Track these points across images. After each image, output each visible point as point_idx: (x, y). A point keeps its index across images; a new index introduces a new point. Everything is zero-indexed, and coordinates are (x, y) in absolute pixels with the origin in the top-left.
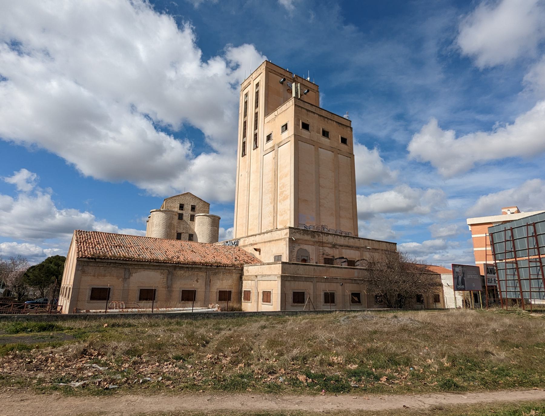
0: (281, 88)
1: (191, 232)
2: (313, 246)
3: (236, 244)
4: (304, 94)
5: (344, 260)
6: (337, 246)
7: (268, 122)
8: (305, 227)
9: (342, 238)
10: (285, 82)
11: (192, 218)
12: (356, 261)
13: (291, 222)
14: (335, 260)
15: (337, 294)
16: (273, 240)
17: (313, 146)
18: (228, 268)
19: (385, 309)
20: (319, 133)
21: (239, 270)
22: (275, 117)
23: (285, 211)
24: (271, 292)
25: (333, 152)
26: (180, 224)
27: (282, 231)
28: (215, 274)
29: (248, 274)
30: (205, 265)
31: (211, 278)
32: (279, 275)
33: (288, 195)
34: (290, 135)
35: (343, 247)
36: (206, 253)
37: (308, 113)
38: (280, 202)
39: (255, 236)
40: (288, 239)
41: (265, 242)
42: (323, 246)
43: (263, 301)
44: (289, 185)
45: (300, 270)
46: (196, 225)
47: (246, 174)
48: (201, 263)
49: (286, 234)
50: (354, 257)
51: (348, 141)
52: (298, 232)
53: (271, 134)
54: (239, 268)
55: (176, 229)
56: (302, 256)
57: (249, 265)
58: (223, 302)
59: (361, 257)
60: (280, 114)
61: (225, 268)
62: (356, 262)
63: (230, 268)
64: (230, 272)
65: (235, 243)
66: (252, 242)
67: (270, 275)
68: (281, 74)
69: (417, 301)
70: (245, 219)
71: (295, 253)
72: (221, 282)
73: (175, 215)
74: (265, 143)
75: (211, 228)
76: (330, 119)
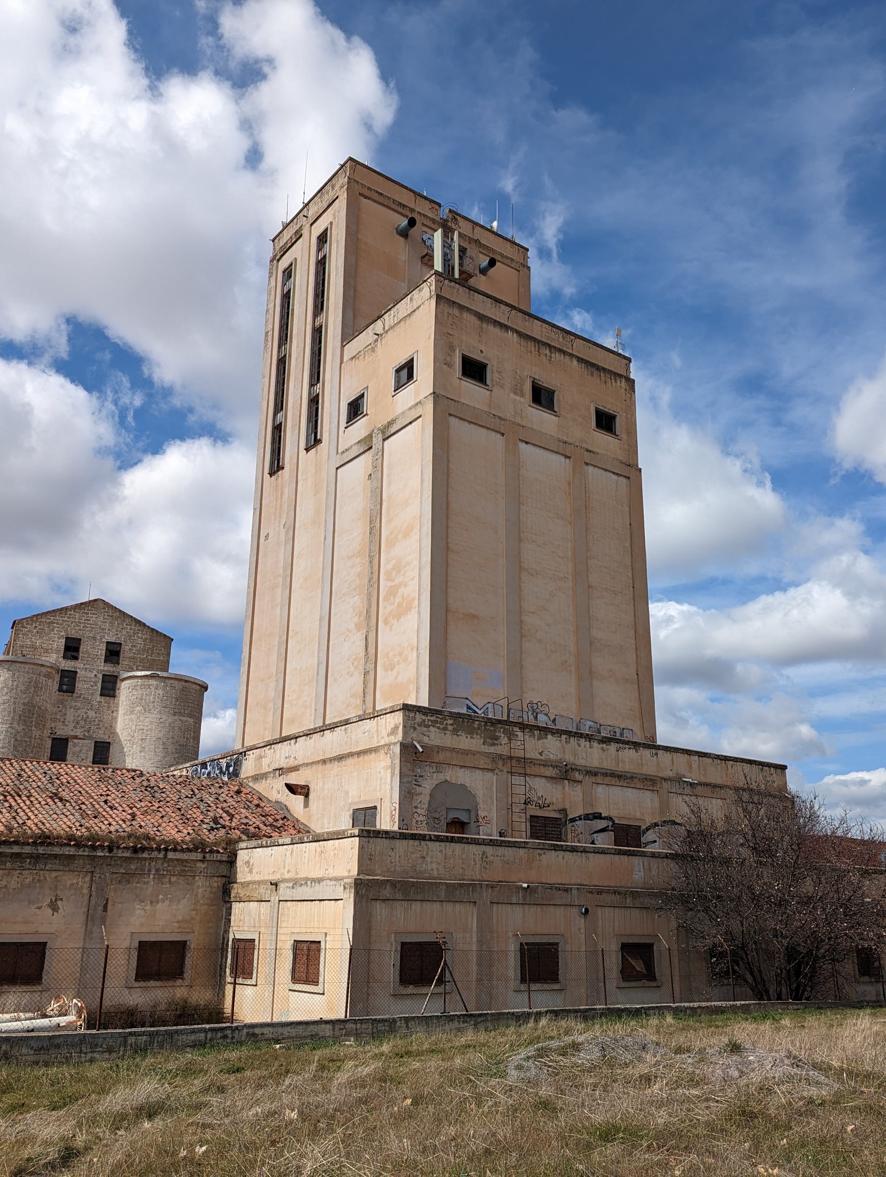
0: (402, 251)
1: (101, 736)
2: (490, 774)
3: (231, 769)
4: (477, 272)
5: (602, 824)
6: (577, 774)
7: (352, 359)
8: (469, 708)
9: (595, 744)
10: (413, 231)
11: (109, 686)
12: (643, 827)
13: (421, 691)
14: (569, 825)
15: (568, 948)
16: (351, 755)
17: (499, 436)
18: (178, 855)
19: (738, 1003)
20: (520, 392)
21: (221, 862)
22: (376, 341)
23: (400, 654)
24: (323, 944)
25: (569, 458)
26: (65, 707)
27: (382, 720)
28: (128, 877)
29: (249, 878)
30: (86, 846)
31: (111, 895)
32: (349, 881)
33: (414, 599)
34: (421, 397)
35: (599, 779)
36: (106, 802)
37: (484, 325)
38: (386, 622)
39: (293, 741)
40: (397, 749)
41: (324, 762)
42: (525, 775)
43: (295, 979)
44: (416, 563)
45: (429, 859)
46: (121, 711)
47: (283, 531)
48: (71, 838)
49: (394, 731)
50: (638, 815)
51: (619, 424)
52: (436, 722)
53: (362, 396)
54: (215, 857)
55: (48, 725)
56: (448, 809)
57: (253, 843)
58: (152, 983)
59: (662, 812)
60: (392, 328)
61: (166, 856)
62: (644, 833)
63: (185, 856)
64: (185, 871)
65: (228, 766)
66: (283, 764)
67: (319, 880)
68: (400, 204)
69: (862, 974)
70: (273, 685)
71: (423, 799)
72: (148, 907)
73: (48, 676)
74: (342, 428)
75: (170, 720)
76: (561, 351)
